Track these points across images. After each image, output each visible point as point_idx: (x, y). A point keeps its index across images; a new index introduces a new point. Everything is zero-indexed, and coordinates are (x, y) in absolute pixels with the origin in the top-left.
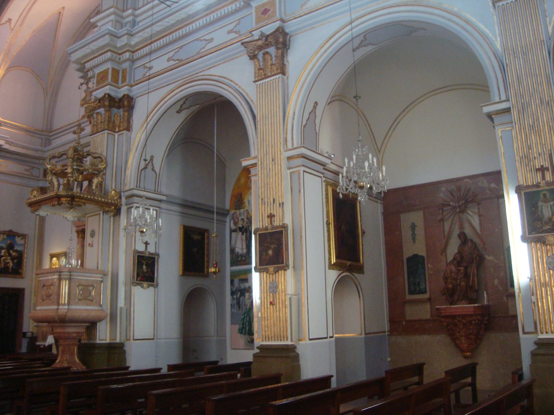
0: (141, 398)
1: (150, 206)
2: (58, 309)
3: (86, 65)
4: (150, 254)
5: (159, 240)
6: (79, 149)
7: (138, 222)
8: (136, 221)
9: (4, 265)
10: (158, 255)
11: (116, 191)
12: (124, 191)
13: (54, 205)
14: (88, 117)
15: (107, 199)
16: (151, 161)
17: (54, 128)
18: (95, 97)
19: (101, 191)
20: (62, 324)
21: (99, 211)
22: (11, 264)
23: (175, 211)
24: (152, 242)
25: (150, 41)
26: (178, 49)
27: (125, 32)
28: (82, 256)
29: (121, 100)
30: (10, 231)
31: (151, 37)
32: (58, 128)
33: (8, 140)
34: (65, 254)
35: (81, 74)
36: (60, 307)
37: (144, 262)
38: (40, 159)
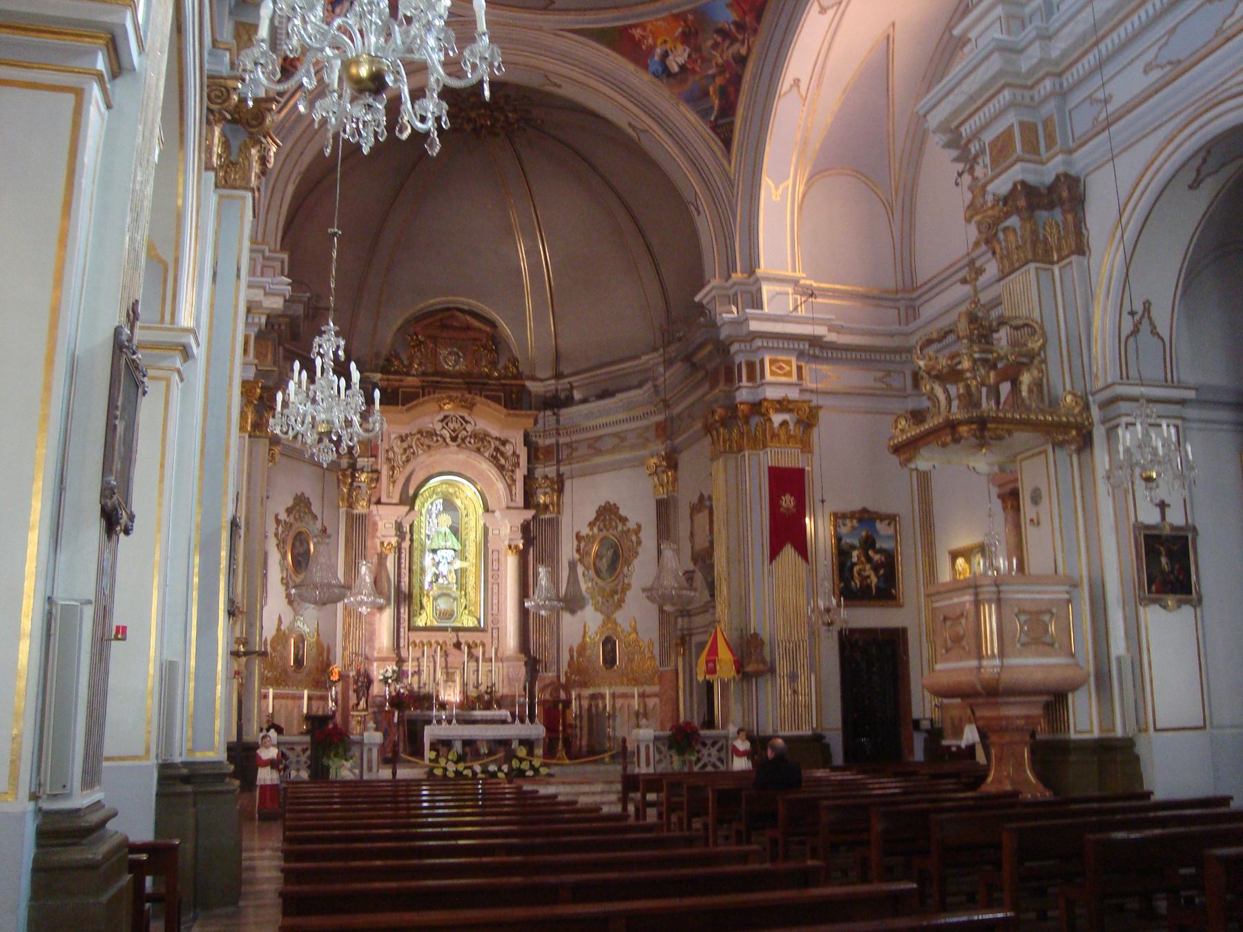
0: (1188, 866)
1: (1159, 417)
2: (979, 668)
3: (962, 129)
4: (1173, 528)
5: (1190, 492)
6: (980, 314)
7: (1137, 457)
8: (1131, 454)
9: (861, 582)
10: (1194, 530)
11: (1074, 395)
12: (1094, 390)
13: (944, 445)
14: (987, 242)
15: (1059, 417)
16: (1146, 315)
17: (920, 281)
18: (994, 195)
19: (1042, 400)
20: (992, 700)
21: (1044, 444)
22: (874, 580)
23: (1226, 423)
24: (1175, 500)
25: (1096, 35)
26: (1166, 38)
27: (1034, 33)
28: (1018, 549)
29: (1052, 188)
30: (864, 511)
31: (1095, 27)
32: (926, 278)
33: (833, 323)
34: (982, 549)
35: (954, 153)
36: (985, 663)
37: (1162, 549)
38: (901, 352)
